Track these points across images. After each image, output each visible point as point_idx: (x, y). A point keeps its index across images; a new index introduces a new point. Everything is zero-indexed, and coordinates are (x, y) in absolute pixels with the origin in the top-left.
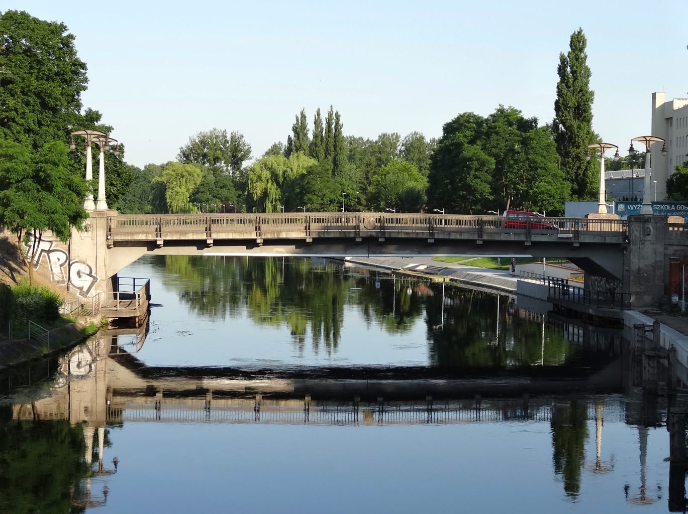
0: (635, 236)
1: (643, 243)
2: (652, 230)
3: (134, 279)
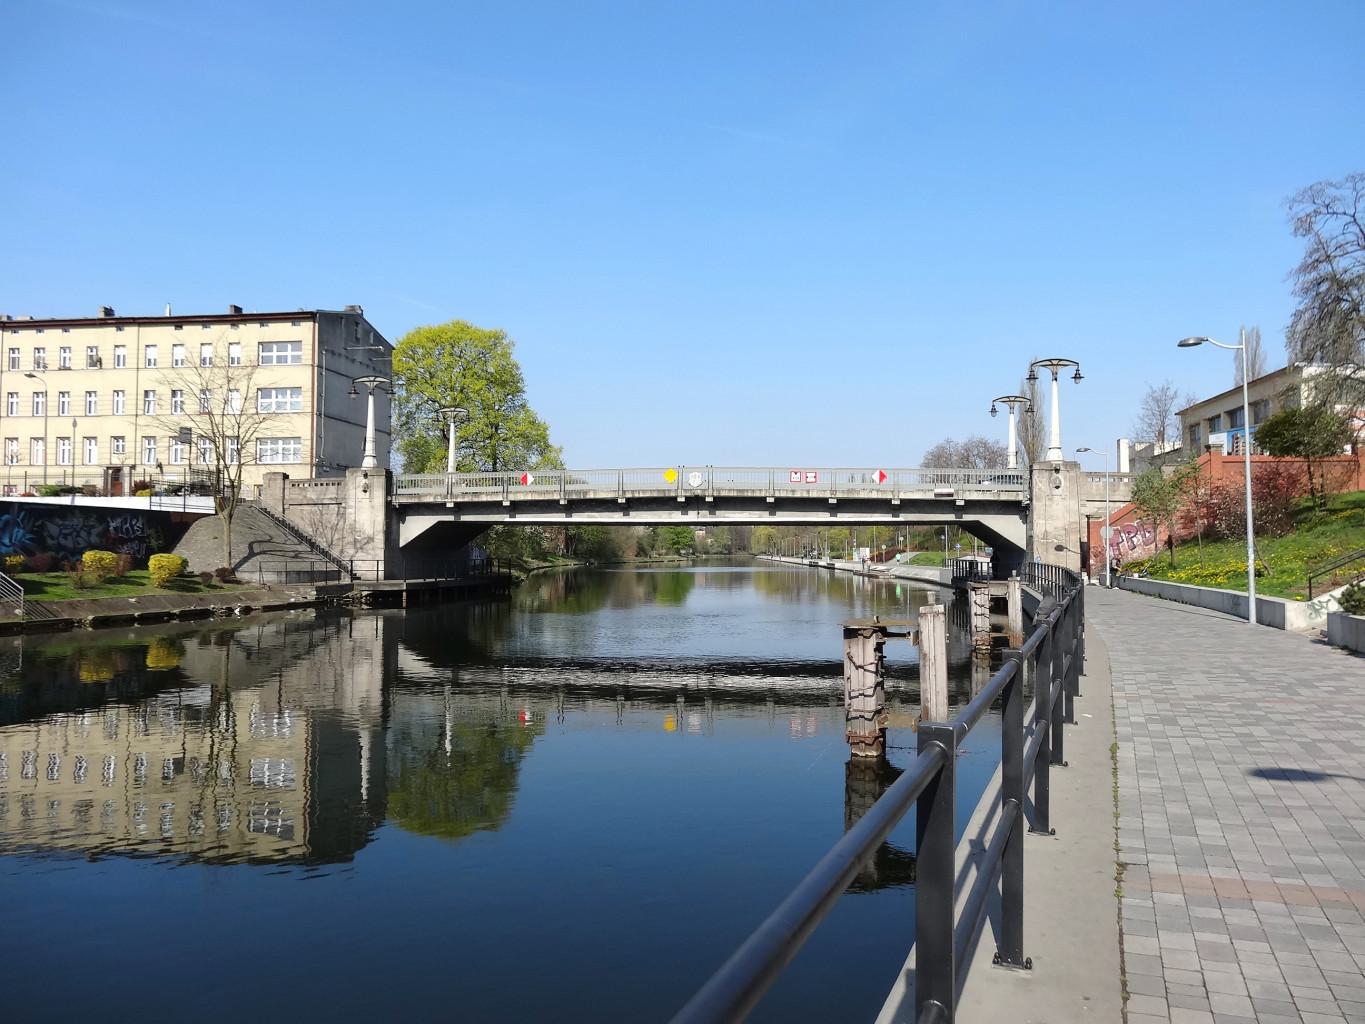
0: (1040, 489)
1: (1051, 497)
2: (1062, 480)
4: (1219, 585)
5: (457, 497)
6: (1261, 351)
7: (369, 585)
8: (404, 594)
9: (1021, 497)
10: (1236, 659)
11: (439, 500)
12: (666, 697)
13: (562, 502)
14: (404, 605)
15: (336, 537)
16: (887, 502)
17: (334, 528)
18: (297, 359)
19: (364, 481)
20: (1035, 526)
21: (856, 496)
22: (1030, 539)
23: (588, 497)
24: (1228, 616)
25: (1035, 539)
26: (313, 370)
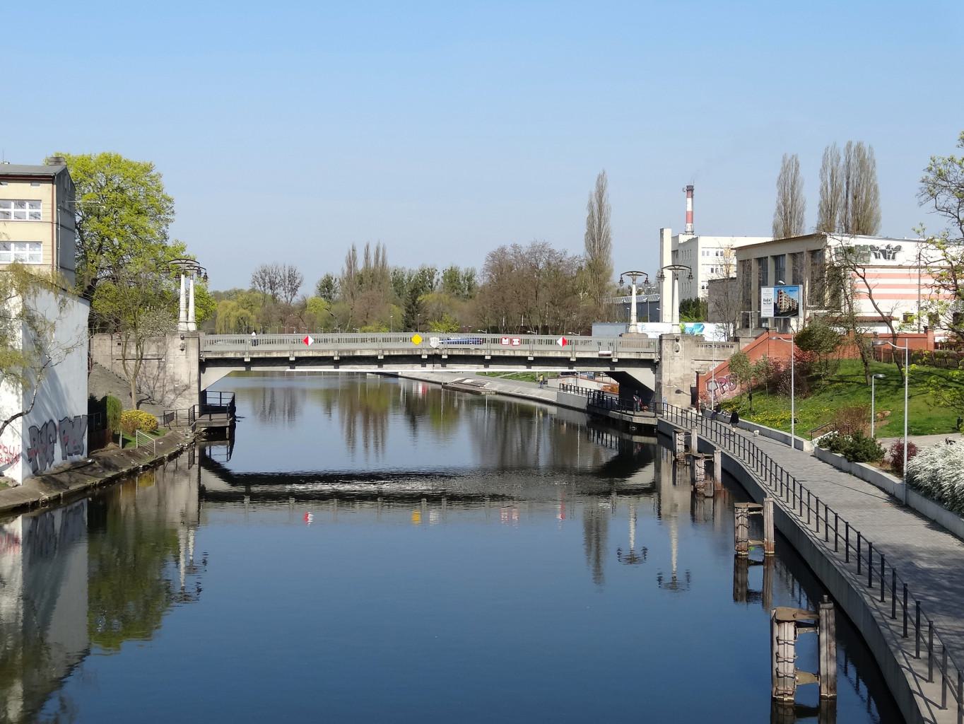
0: (667, 352)
2: (680, 347)
4: (778, 428)
5: (253, 354)
6: (798, 178)
7: (206, 423)
8: (227, 429)
9: (653, 357)
10: (789, 462)
11: (239, 356)
12: (414, 499)
13: (336, 358)
14: (227, 437)
15: (158, 384)
16: (568, 359)
17: (157, 379)
18: (35, 216)
19: (181, 341)
20: (663, 377)
21: (546, 355)
22: (658, 385)
23: (356, 354)
24: (783, 444)
25: (663, 385)
26: (53, 226)
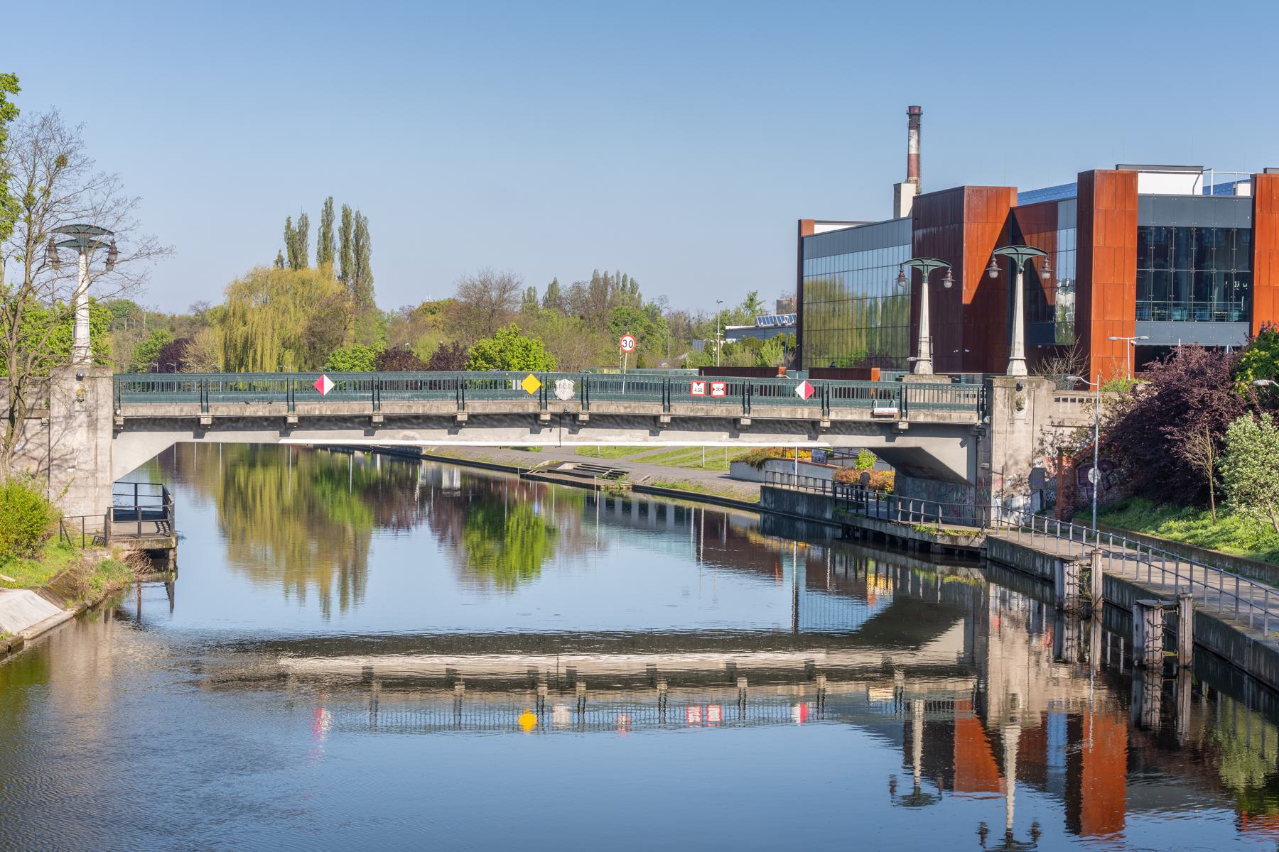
3: (136, 484)
